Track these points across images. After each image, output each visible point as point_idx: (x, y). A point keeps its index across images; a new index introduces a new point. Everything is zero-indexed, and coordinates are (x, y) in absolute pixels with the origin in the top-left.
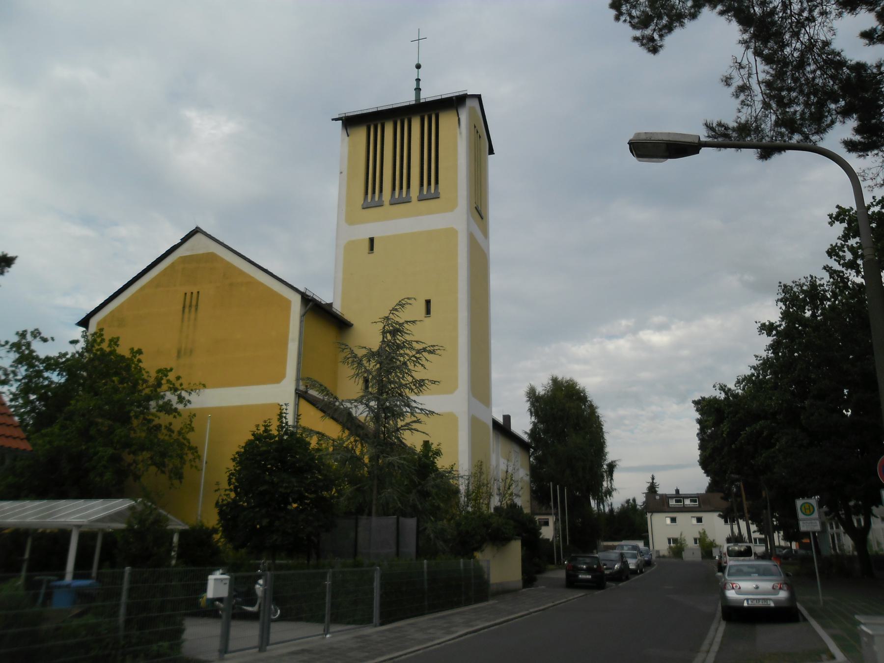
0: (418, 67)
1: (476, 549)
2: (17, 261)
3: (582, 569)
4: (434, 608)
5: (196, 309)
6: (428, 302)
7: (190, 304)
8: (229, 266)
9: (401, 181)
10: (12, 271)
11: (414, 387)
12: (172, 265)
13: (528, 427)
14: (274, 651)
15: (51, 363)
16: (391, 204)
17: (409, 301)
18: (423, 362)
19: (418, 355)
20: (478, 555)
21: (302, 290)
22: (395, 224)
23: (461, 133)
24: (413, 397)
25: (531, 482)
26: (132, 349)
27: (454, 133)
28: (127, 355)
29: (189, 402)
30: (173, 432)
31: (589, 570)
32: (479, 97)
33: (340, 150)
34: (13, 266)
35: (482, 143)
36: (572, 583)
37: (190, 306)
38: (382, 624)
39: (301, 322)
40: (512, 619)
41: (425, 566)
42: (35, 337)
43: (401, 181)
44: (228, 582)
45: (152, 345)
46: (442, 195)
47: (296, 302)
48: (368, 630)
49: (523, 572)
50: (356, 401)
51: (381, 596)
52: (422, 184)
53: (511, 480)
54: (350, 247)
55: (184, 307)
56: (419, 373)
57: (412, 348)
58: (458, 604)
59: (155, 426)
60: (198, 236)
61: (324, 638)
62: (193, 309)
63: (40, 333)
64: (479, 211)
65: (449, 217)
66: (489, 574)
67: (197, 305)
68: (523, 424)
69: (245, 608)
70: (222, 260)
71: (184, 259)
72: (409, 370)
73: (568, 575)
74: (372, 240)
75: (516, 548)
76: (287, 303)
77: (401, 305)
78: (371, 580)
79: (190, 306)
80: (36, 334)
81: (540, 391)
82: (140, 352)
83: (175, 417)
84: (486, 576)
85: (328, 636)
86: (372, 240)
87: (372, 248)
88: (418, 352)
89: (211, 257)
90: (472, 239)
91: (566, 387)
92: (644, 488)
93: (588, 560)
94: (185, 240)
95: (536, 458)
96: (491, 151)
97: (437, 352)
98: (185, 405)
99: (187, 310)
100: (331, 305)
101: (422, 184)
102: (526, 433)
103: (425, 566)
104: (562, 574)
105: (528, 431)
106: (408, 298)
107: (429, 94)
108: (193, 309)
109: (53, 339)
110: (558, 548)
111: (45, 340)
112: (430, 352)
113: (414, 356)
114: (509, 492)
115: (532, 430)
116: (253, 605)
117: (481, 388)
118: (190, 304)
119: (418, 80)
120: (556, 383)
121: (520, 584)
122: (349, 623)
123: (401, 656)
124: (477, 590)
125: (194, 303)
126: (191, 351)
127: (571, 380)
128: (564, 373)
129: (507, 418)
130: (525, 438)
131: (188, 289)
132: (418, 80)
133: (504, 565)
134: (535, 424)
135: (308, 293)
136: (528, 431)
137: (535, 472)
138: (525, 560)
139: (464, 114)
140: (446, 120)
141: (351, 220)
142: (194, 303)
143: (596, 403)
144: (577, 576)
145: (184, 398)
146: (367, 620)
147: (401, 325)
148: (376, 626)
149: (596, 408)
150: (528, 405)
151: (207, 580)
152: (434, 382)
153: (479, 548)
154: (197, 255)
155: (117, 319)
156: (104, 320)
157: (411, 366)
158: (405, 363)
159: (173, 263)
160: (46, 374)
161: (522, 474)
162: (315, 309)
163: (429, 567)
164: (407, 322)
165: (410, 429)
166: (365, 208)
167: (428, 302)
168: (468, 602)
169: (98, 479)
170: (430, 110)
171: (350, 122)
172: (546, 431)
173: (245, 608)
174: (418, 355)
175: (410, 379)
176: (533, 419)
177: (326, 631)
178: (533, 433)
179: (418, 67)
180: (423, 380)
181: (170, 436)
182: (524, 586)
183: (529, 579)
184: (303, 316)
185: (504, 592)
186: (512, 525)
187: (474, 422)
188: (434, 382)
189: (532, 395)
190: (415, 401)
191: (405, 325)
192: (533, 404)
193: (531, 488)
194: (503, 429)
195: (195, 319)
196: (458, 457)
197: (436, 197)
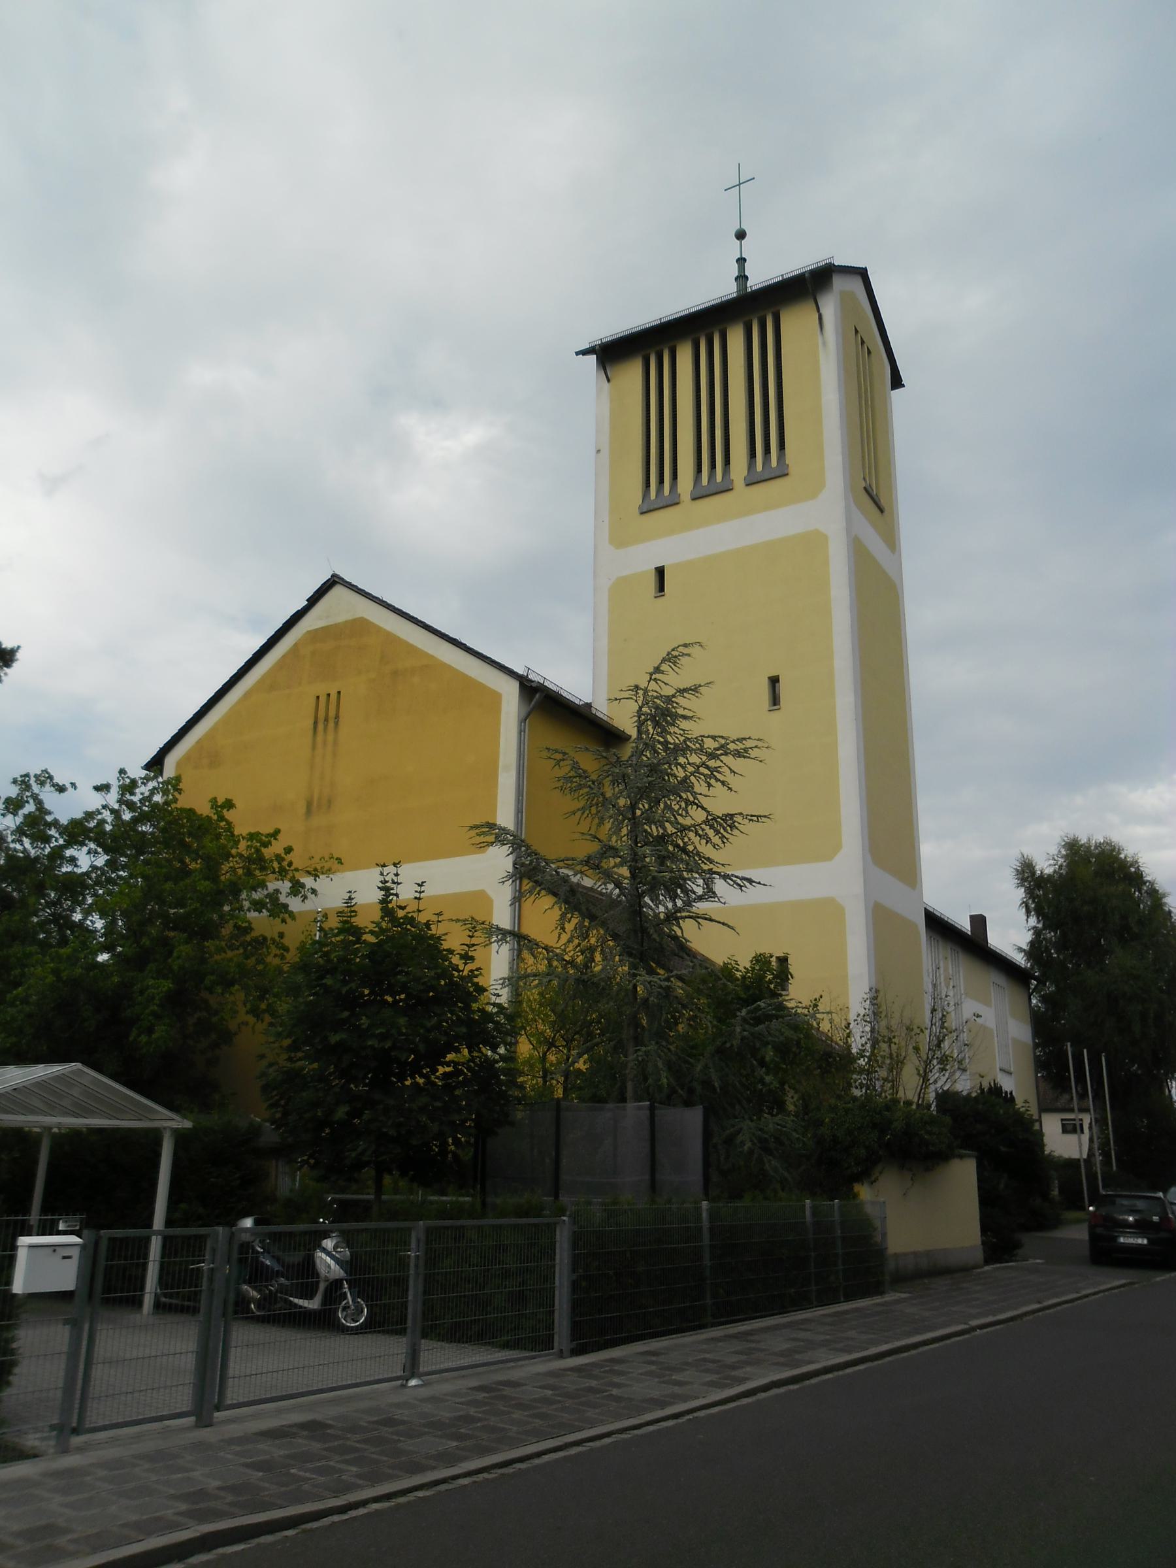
0: (741, 235)
1: (859, 1178)
2: (19, 655)
3: (1127, 1225)
4: (728, 1313)
5: (337, 724)
6: (774, 681)
7: (326, 716)
8: (391, 639)
9: (712, 452)
10: (13, 673)
11: (711, 833)
12: (295, 649)
13: (1024, 938)
14: (232, 1424)
15: (77, 832)
16: (694, 499)
17: (686, 651)
18: (729, 778)
19: (712, 763)
20: (864, 1192)
21: (521, 671)
22: (706, 536)
23: (824, 344)
24: (706, 850)
25: (1036, 1046)
26: (214, 801)
27: (813, 348)
28: (204, 810)
29: (314, 892)
30: (287, 950)
31: (1142, 1227)
32: (862, 274)
33: (594, 409)
34: (16, 665)
35: (875, 365)
36: (1105, 1253)
37: (326, 720)
38: (575, 1352)
39: (521, 731)
40: (915, 1346)
41: (808, 1213)
42: (42, 784)
43: (712, 452)
44: (75, 1253)
45: (257, 796)
46: (792, 470)
47: (510, 691)
48: (532, 1369)
49: (984, 1229)
50: (581, 863)
51: (575, 1286)
52: (752, 454)
53: (942, 1027)
54: (621, 589)
55: (316, 723)
56: (718, 801)
57: (701, 749)
58: (800, 1302)
59: (256, 940)
60: (338, 590)
61: (404, 1386)
62: (331, 724)
63: (51, 778)
64: (873, 494)
65: (814, 509)
66: (884, 1235)
67: (337, 717)
68: (1012, 934)
69: (296, 1301)
70: (379, 629)
71: (314, 636)
72: (694, 794)
73: (1094, 1238)
74: (660, 572)
75: (963, 1177)
76: (495, 698)
77: (671, 658)
78: (549, 1252)
79: (326, 720)
80: (45, 778)
81: (1045, 866)
82: (229, 805)
83: (284, 921)
84: (878, 1238)
85: (413, 1382)
86: (660, 572)
87: (661, 587)
88: (712, 756)
89: (359, 627)
90: (860, 555)
91: (1098, 856)
92: (731, 729)
93: (1140, 1204)
94: (313, 601)
95: (1044, 999)
96: (897, 382)
97: (752, 753)
98: (305, 898)
99: (321, 727)
100: (589, 705)
101: (752, 454)
102: (1020, 949)
103: (808, 1213)
104: (1077, 1233)
105: (1025, 947)
106: (686, 645)
107: (760, 276)
108: (331, 724)
109: (73, 785)
110: (1092, 1177)
111: (61, 789)
112: (738, 754)
113: (703, 764)
114: (938, 1054)
115: (1032, 943)
116: (310, 1296)
117: (892, 842)
118: (326, 716)
119: (741, 261)
120: (1074, 851)
121: (979, 1255)
122: (506, 1346)
123: (539, 1455)
124: (857, 1268)
125: (332, 713)
126: (330, 802)
127: (1108, 843)
128: (1093, 830)
129: (979, 922)
130: (1020, 959)
131: (321, 689)
132: (741, 261)
133: (933, 1214)
134: (1037, 932)
135: (532, 677)
136: (1025, 947)
137: (1042, 1026)
138: (988, 1199)
139: (829, 306)
140: (796, 324)
141: (620, 538)
142: (332, 713)
143: (1162, 884)
144: (1115, 1238)
145: (303, 886)
146: (541, 1343)
147: (669, 699)
148: (561, 1355)
149: (1164, 895)
150: (1021, 893)
151: (14, 1248)
152: (756, 818)
153: (864, 1174)
154: (336, 625)
155: (208, 755)
156: (187, 757)
157: (700, 787)
158: (685, 784)
159: (296, 645)
160: (68, 853)
161: (1020, 1031)
162: (542, 701)
163: (713, 1215)
164: (682, 691)
165: (695, 917)
166: (646, 510)
167: (774, 681)
168: (827, 1296)
169: (144, 1038)
170: (758, 307)
171: (610, 353)
172: (1062, 945)
173: (296, 1301)
174: (712, 763)
175: (700, 816)
176: (1033, 921)
177: (412, 1368)
178: (1035, 950)
179: (741, 235)
180: (732, 816)
181: (283, 957)
182: (987, 1261)
183: (1000, 1243)
184: (523, 721)
185: (930, 1272)
186: (986, 1130)
187: (882, 920)
188: (756, 818)
189: (1027, 874)
190: (710, 861)
191: (679, 700)
192: (1030, 893)
193: (1037, 1059)
194: (969, 943)
195: (335, 743)
196: (838, 987)
197: (782, 473)
